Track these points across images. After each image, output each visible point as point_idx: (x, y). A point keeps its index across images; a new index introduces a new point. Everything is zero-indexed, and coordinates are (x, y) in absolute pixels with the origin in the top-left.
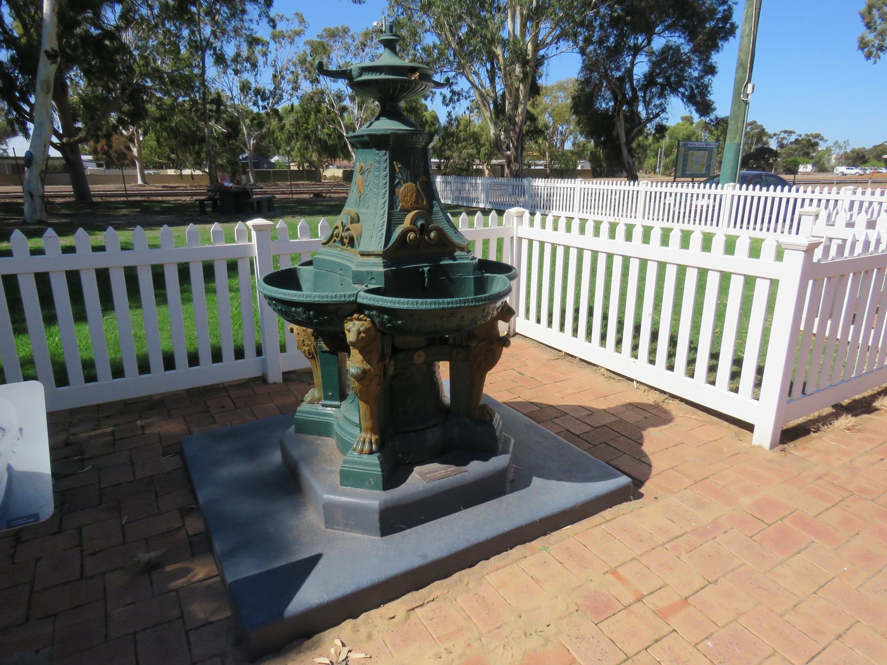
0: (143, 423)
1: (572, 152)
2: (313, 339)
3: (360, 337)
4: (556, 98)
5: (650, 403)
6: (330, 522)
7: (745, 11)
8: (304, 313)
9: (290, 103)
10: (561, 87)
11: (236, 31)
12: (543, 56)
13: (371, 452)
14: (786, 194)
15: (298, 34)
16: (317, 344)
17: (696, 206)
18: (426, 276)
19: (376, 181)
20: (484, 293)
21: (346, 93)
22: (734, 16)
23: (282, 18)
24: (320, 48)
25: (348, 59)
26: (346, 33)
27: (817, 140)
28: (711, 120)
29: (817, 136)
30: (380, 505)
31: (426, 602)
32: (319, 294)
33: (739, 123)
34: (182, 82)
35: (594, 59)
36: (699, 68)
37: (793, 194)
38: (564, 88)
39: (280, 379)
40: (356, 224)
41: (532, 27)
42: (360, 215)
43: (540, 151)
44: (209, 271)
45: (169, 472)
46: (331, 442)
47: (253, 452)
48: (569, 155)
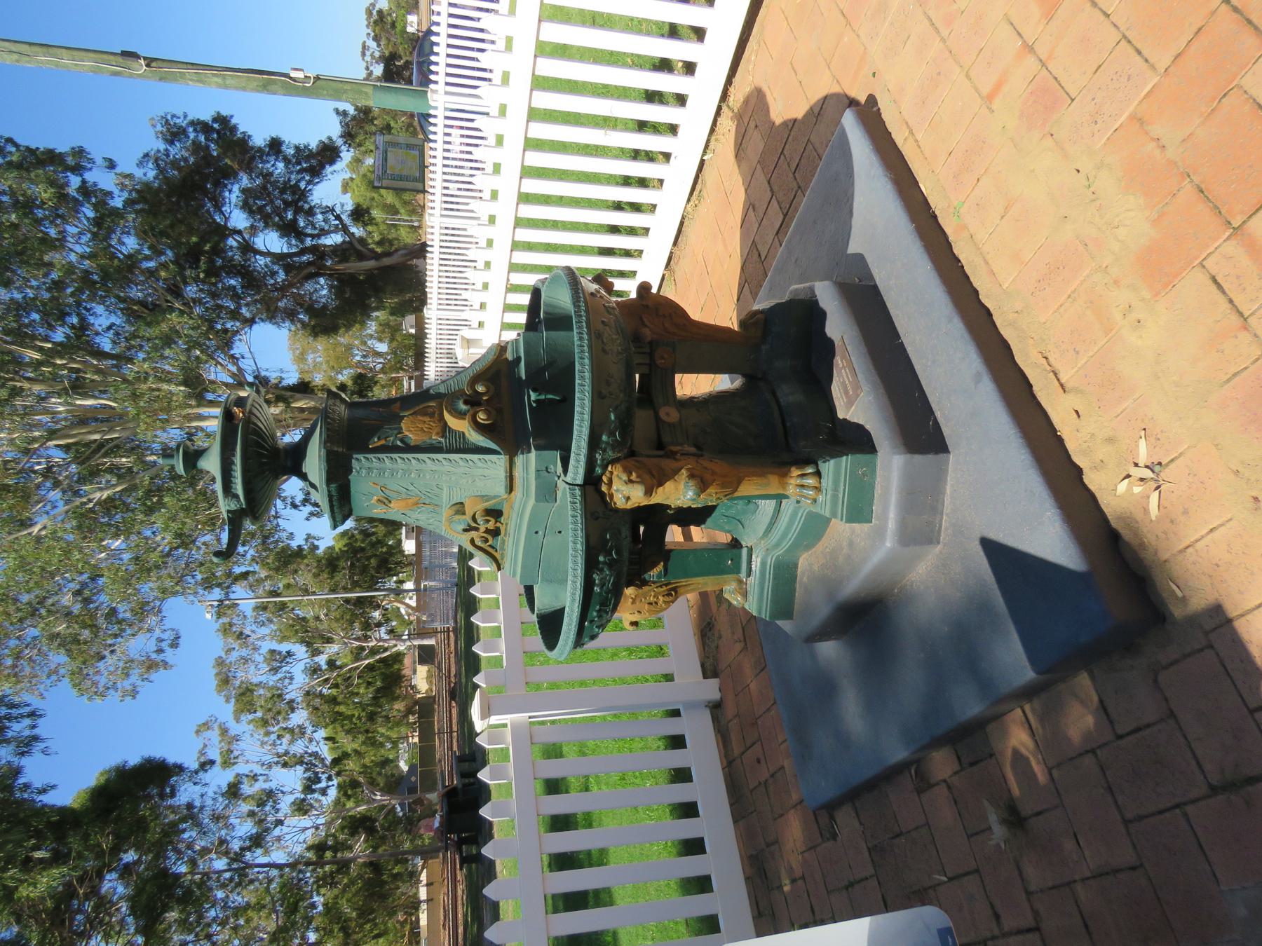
0: (787, 882)
1: (392, 339)
2: (646, 588)
3: (638, 480)
4: (315, 364)
5: (734, 127)
6: (930, 538)
7: (190, 83)
8: (601, 570)
9: (322, 742)
10: (301, 358)
11: (216, 818)
12: (256, 377)
13: (818, 474)
14: (443, 30)
15: (224, 731)
16: (654, 583)
17: (462, 152)
18: (543, 397)
20: (572, 317)
21: (308, 660)
22: (202, 118)
23: (202, 753)
24: (245, 698)
25: (260, 659)
26: (223, 661)
27: (374, 13)
28: (345, 143)
29: (369, 12)
30: (900, 454)
31: (1049, 368)
32: (571, 544)
33: (345, 87)
34: (291, 896)
35: (259, 306)
36: (272, 163)
37: (443, 20)
38: (302, 354)
39: (714, 683)
40: (466, 506)
41: (214, 392)
42: (451, 503)
43: (391, 386)
44: (561, 823)
45: (861, 824)
46: (807, 563)
47: (825, 688)
48: (395, 344)
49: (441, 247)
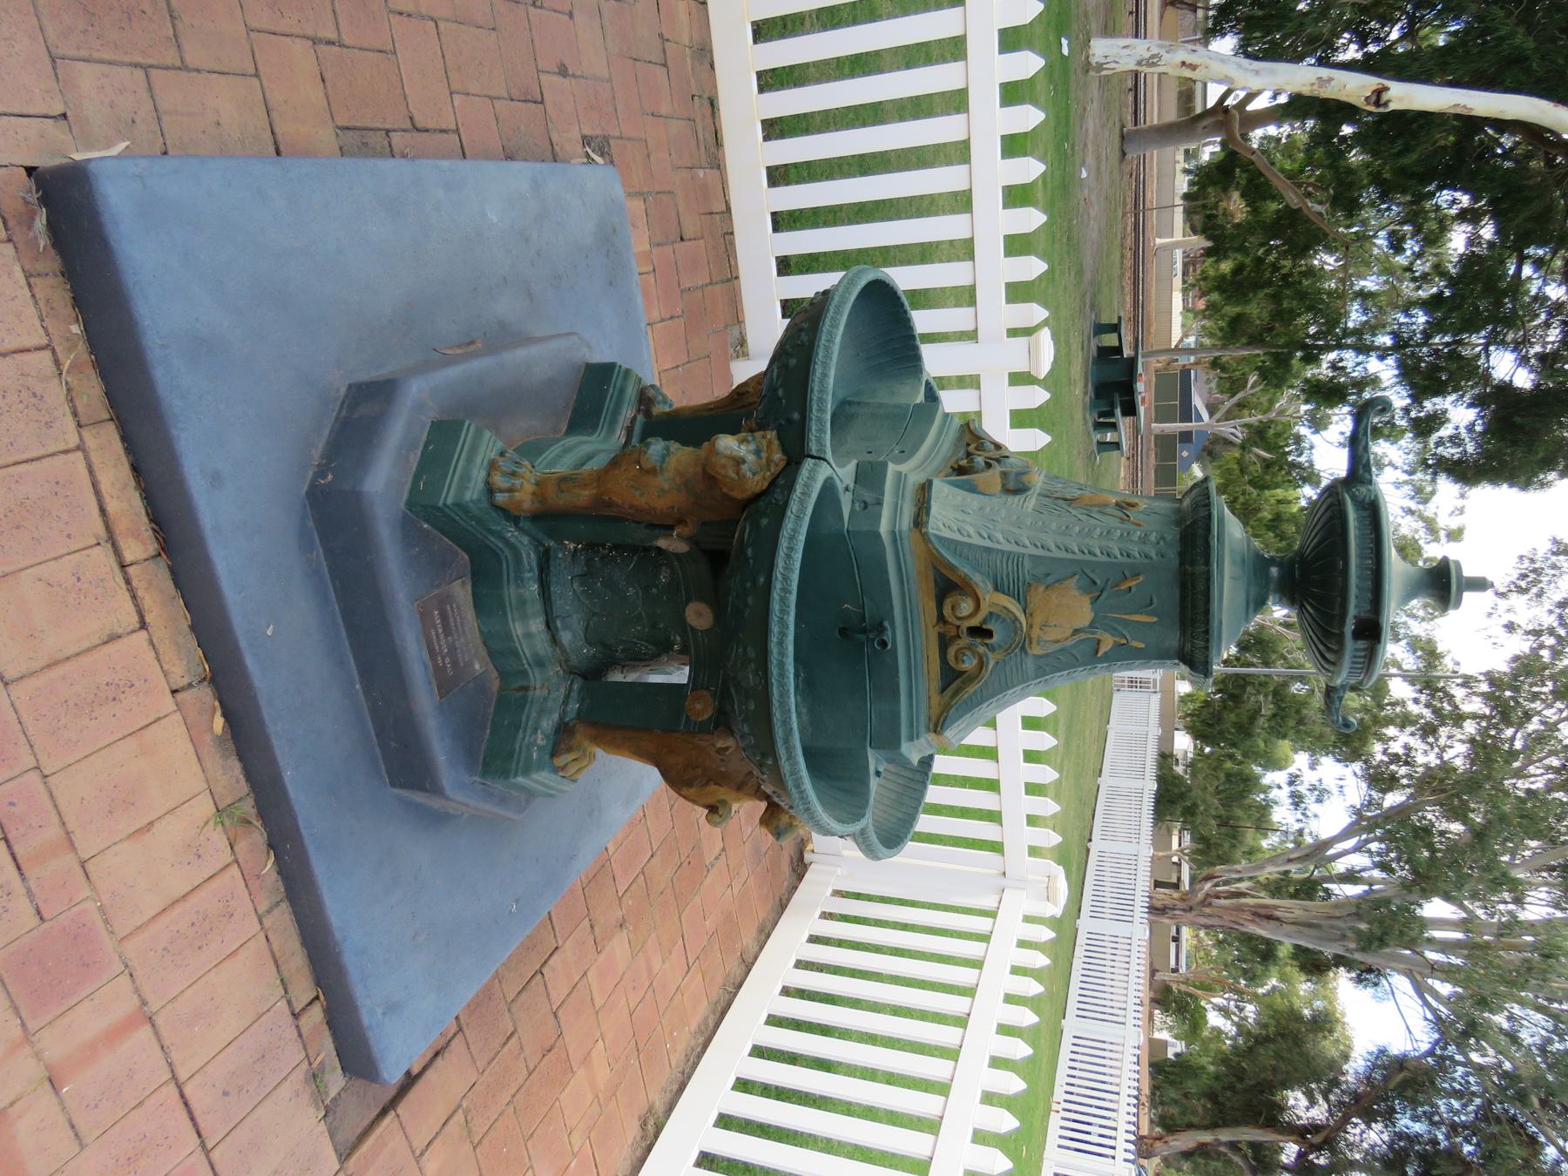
13: (490, 490)
19: (1098, 531)
49: (1114, 1148)
